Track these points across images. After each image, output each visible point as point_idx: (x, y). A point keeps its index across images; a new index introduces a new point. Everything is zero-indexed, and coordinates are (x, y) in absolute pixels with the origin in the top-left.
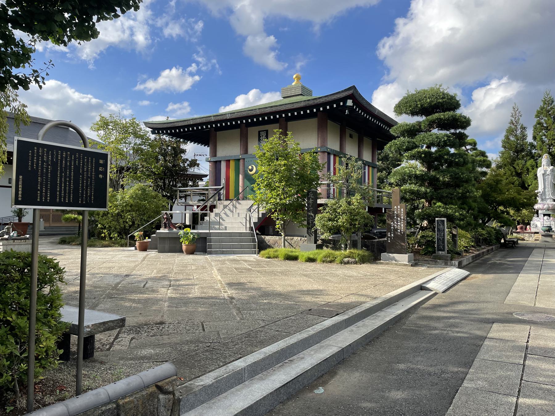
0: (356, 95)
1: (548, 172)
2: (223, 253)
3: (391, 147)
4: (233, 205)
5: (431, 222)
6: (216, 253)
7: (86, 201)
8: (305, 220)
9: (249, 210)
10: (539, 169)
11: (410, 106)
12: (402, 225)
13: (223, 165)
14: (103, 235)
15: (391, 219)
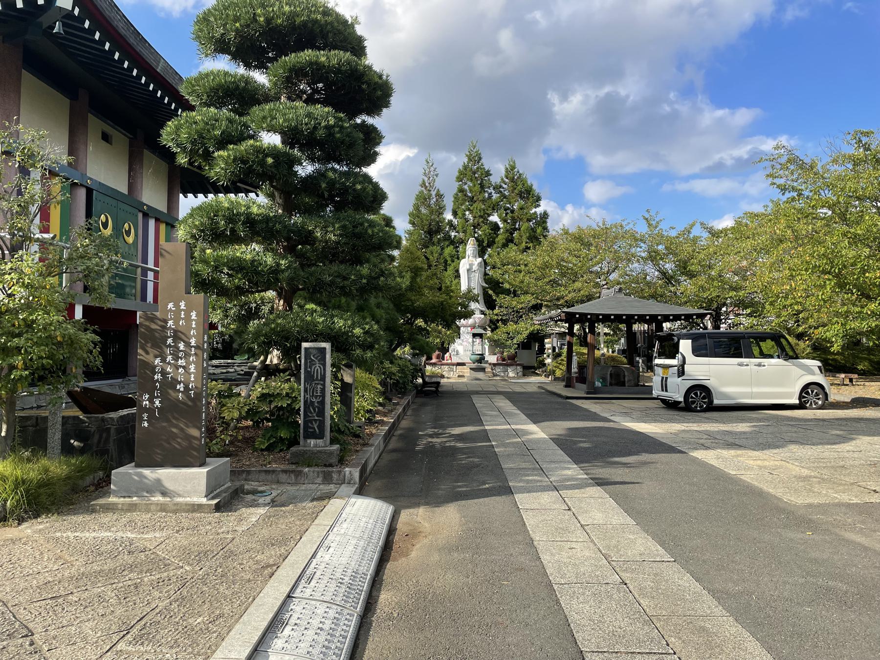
1: (475, 267)
3: (178, 128)
5: (290, 353)
10: (463, 262)
12: (192, 368)
15: (155, 345)
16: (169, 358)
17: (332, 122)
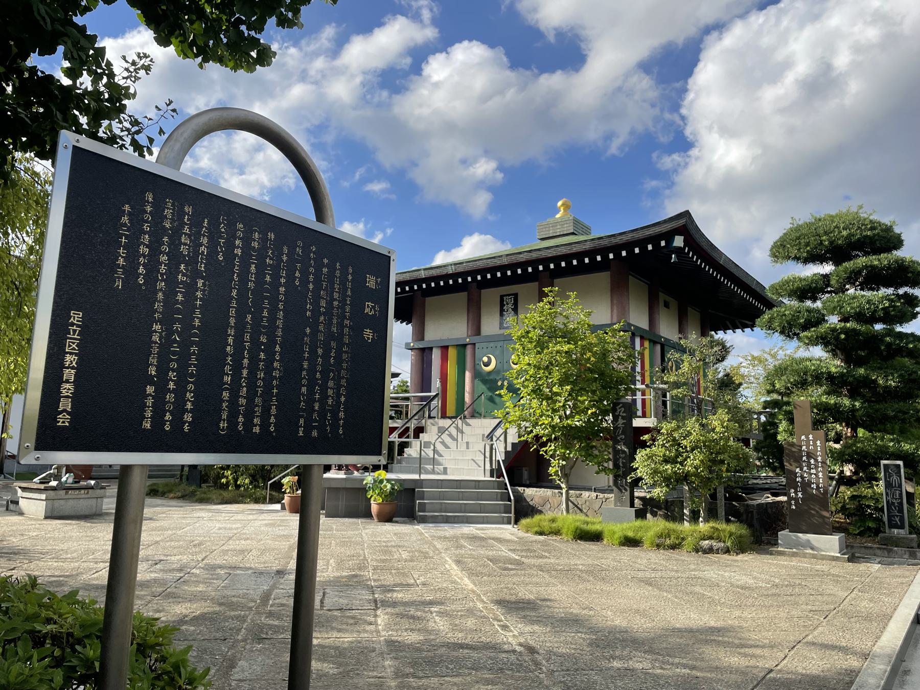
0: (690, 227)
2: (447, 520)
4: (457, 428)
6: (435, 520)
7: (321, 429)
8: (609, 459)
9: (490, 436)
11: (807, 244)
12: (820, 475)
13: (436, 355)
14: (224, 480)
16: (805, 468)
17: (887, 305)
